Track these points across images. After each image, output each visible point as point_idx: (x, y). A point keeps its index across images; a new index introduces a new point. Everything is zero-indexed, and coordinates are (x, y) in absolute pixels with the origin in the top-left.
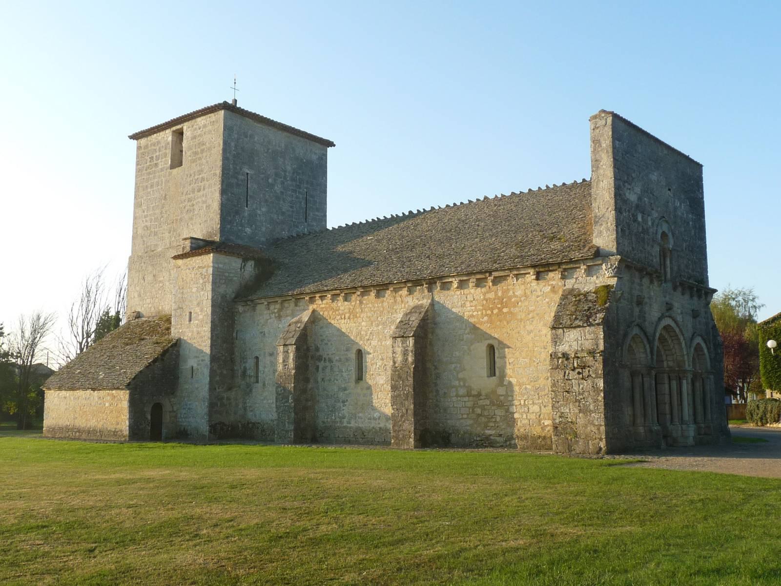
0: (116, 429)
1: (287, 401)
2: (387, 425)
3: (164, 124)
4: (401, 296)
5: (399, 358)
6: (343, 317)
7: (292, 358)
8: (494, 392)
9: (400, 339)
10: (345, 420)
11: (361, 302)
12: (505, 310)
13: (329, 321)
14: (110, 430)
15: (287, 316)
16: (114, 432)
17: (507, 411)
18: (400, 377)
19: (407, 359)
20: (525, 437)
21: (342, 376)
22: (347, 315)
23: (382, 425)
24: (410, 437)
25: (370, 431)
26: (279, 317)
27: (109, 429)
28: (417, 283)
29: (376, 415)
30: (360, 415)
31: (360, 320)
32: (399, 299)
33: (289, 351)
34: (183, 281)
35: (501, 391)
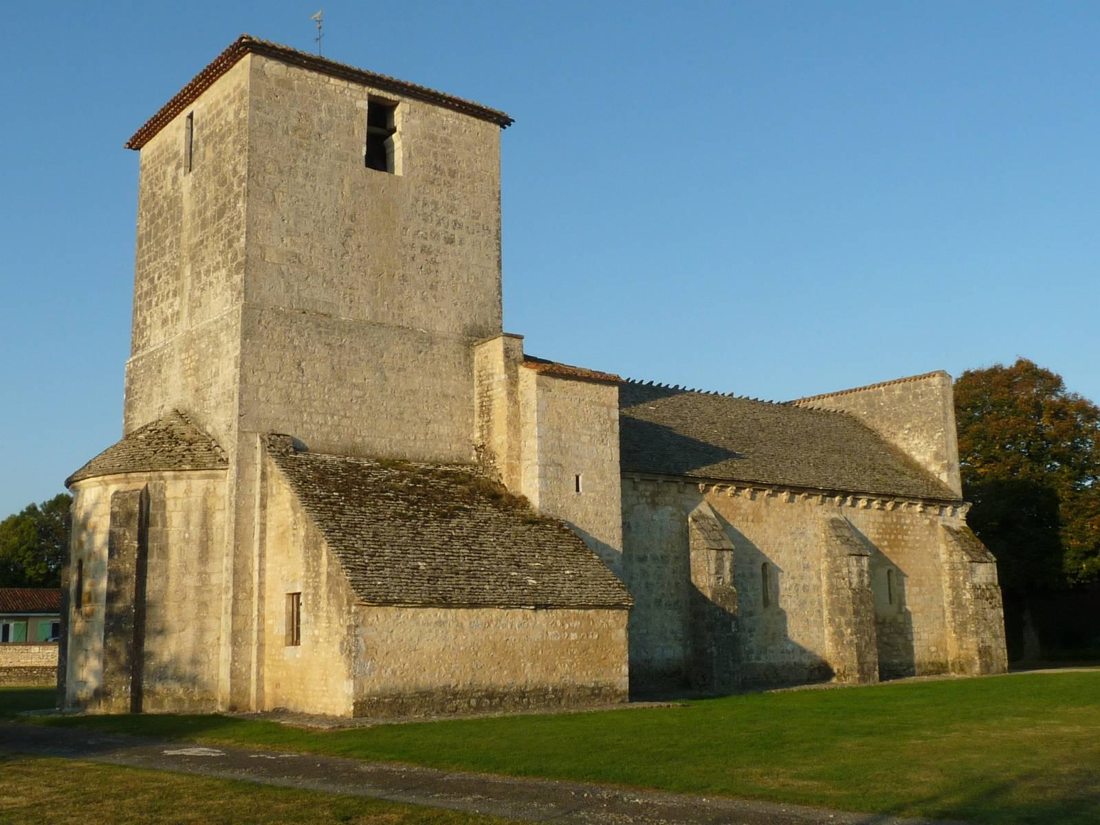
0: (596, 683)
1: (730, 630)
2: (802, 659)
3: (413, 87)
4: (810, 505)
5: (855, 580)
6: (745, 518)
7: (728, 569)
8: (895, 619)
9: (854, 557)
10: (753, 656)
11: (767, 504)
12: (900, 537)
13: (728, 520)
14: (582, 686)
15: (666, 505)
16: (593, 689)
17: (906, 638)
18: (862, 602)
19: (862, 581)
20: (920, 665)
21: (747, 596)
22: (751, 518)
23: (796, 659)
24: (875, 670)
25: (783, 667)
26: (654, 505)
27: (578, 683)
28: (832, 493)
29: (789, 647)
30: (771, 648)
31: (765, 526)
32: (807, 508)
33: (725, 559)
34: (560, 418)
35: (901, 619)
